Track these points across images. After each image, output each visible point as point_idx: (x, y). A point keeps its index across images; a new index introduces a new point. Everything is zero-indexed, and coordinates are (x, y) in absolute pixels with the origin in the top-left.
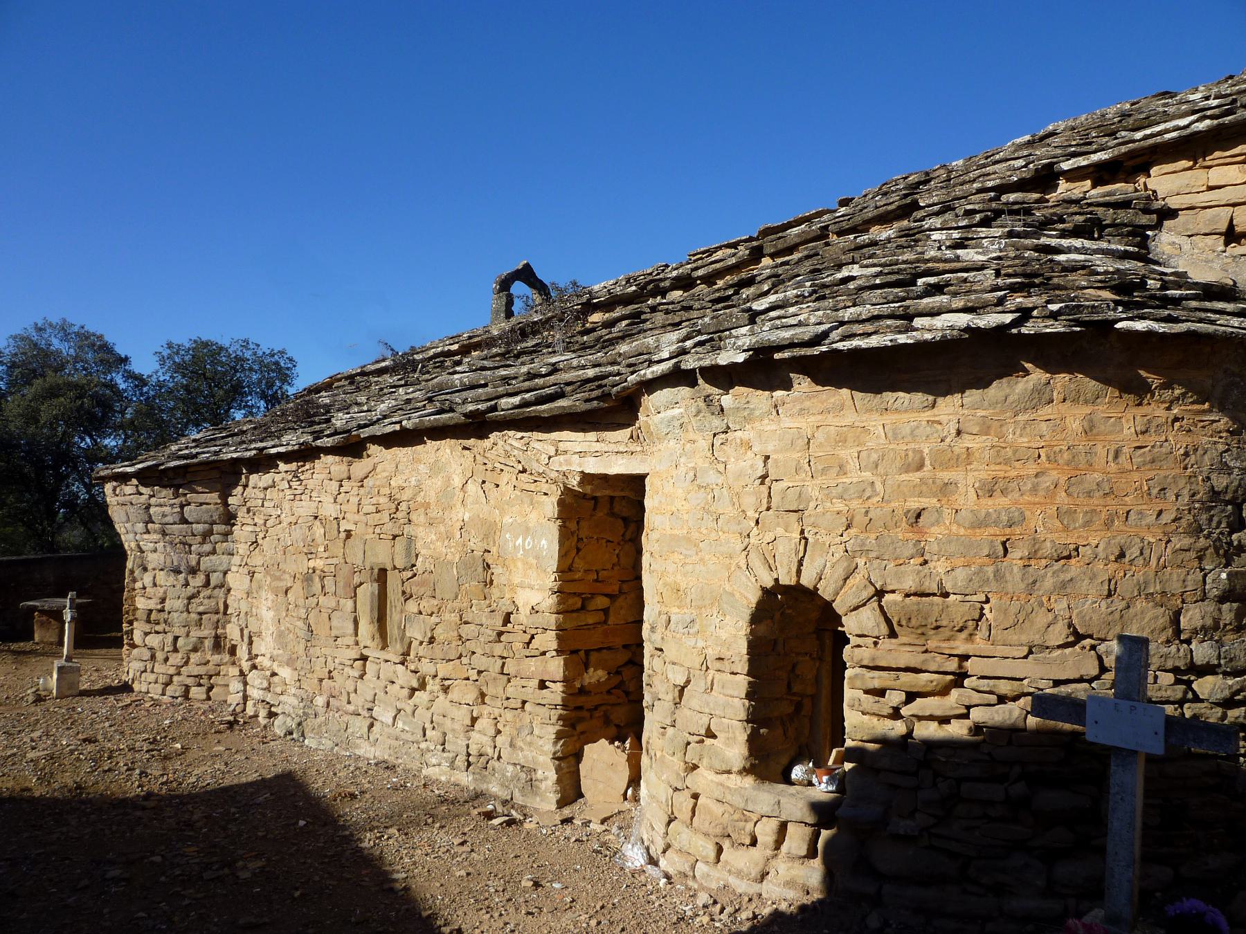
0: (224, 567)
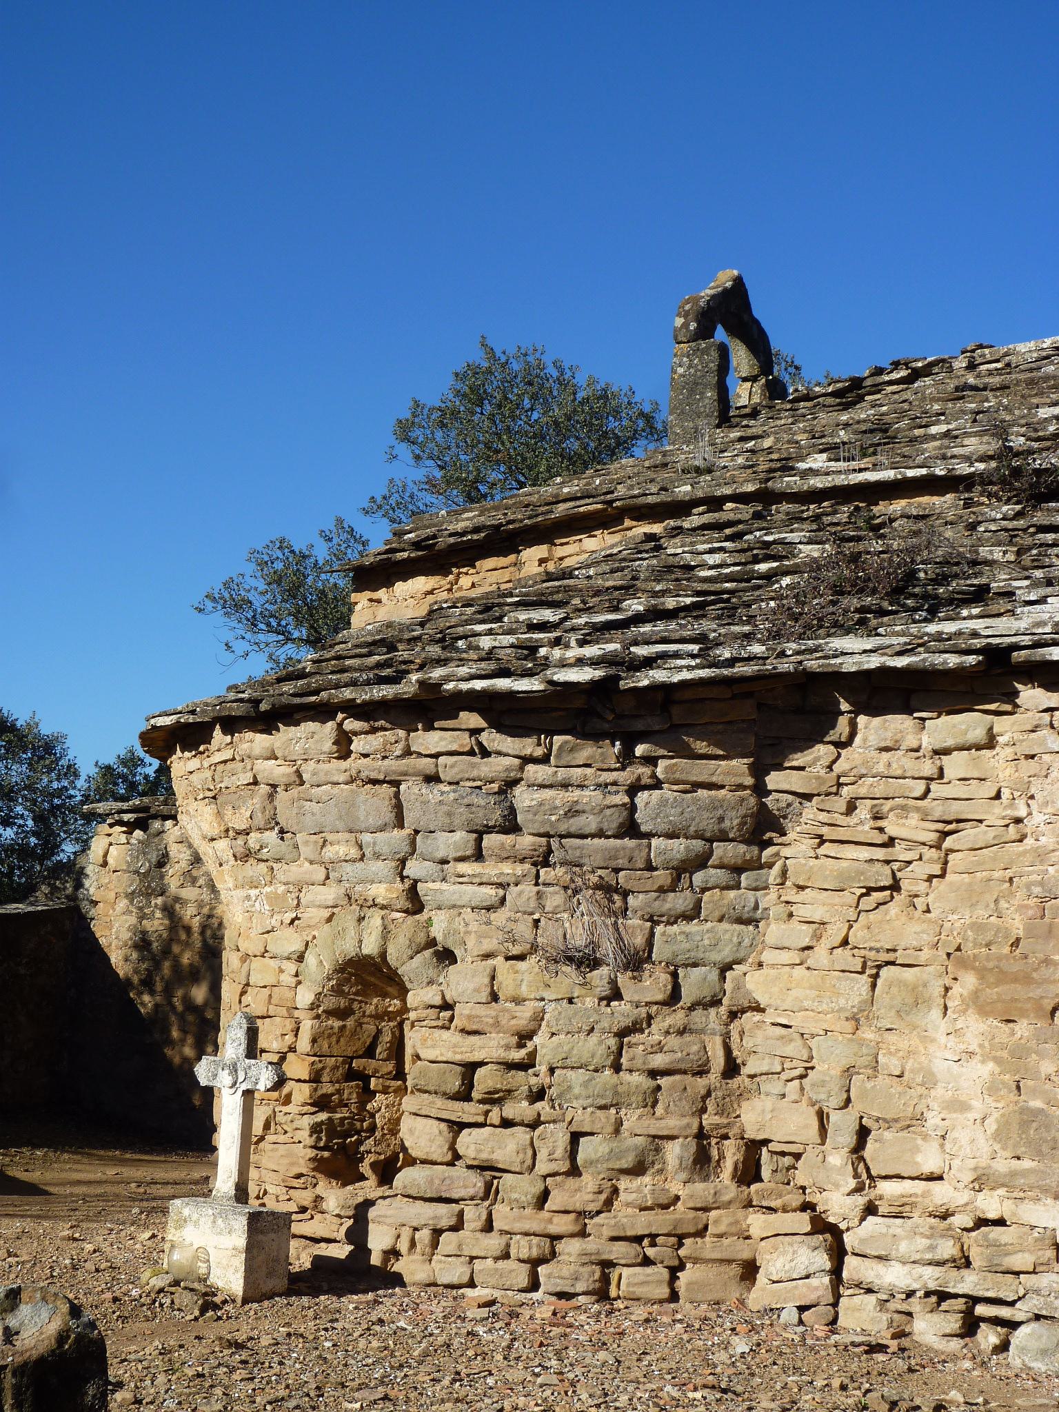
0: (725, 954)
